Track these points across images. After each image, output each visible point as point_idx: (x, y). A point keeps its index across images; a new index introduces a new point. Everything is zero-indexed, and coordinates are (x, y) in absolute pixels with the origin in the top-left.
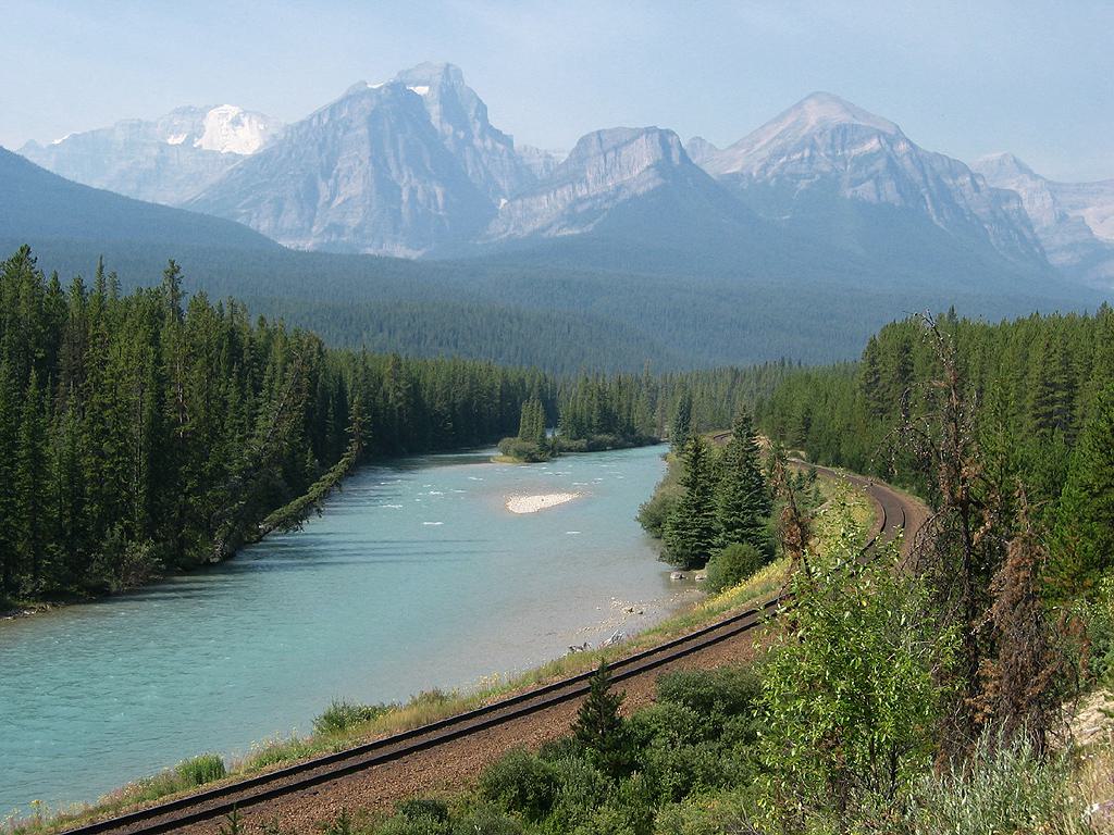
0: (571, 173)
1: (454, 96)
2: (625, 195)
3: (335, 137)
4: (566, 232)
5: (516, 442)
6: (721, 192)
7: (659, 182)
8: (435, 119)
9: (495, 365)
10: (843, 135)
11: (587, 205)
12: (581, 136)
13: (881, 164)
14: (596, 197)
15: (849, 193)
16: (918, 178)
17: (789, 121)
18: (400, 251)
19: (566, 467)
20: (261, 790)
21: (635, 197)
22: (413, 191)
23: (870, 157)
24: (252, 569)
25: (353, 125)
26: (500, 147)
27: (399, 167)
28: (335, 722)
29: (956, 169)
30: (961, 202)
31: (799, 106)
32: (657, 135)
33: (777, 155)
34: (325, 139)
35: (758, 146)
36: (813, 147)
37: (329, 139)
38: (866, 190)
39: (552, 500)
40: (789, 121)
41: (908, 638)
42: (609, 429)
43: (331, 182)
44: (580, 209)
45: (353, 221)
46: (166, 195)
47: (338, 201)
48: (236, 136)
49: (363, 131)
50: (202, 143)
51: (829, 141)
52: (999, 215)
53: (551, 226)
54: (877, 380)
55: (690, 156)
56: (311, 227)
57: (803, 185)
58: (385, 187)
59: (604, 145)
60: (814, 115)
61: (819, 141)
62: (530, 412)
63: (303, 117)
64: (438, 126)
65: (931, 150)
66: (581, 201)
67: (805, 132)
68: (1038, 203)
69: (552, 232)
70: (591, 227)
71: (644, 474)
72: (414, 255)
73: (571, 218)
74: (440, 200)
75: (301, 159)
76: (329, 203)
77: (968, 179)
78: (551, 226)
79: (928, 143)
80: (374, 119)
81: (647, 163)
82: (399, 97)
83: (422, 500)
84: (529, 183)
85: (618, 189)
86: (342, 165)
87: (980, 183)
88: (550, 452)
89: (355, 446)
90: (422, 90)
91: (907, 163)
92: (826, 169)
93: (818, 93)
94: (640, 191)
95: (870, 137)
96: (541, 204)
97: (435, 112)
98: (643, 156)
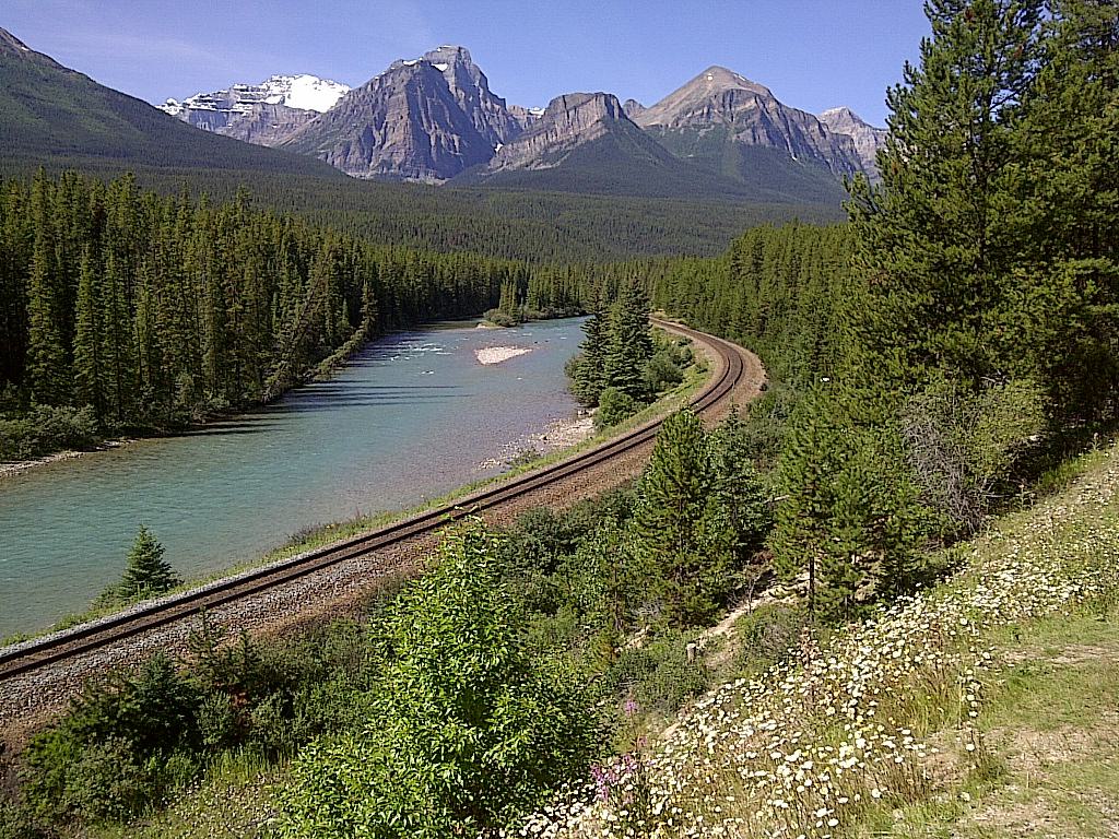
2: (581, 140)
3: (383, 99)
5: (497, 313)
6: (647, 139)
7: (604, 131)
8: (452, 88)
9: (450, 264)
10: (730, 97)
11: (556, 148)
13: (756, 118)
14: (562, 143)
16: (782, 127)
19: (529, 331)
22: (438, 138)
23: (749, 113)
24: (298, 409)
25: (396, 91)
26: (497, 107)
27: (429, 121)
28: (300, 540)
29: (808, 119)
30: (811, 144)
31: (701, 76)
32: (603, 98)
34: (377, 100)
35: (672, 106)
36: (710, 106)
37: (380, 101)
38: (746, 137)
39: (522, 352)
40: (693, 88)
42: (562, 306)
43: (382, 132)
44: (551, 151)
45: (398, 159)
47: (387, 144)
48: (314, 95)
49: (402, 96)
51: (721, 101)
52: (838, 152)
54: (739, 271)
55: (626, 112)
56: (370, 162)
57: (702, 133)
58: (419, 136)
59: (566, 105)
60: (712, 84)
61: (714, 102)
62: (507, 292)
63: (361, 85)
64: (454, 92)
66: (553, 145)
67: (705, 95)
68: (865, 143)
71: (569, 337)
73: (545, 156)
74: (456, 144)
77: (817, 127)
80: (410, 87)
81: (596, 119)
82: (427, 66)
83: (429, 350)
84: (515, 131)
86: (389, 119)
87: (825, 130)
88: (521, 320)
89: (367, 321)
90: (442, 67)
91: (775, 116)
93: (714, 67)
94: (592, 139)
95: (749, 98)
96: (524, 147)
97: (451, 80)
98: (595, 111)
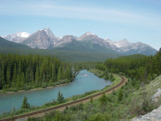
0: (62, 40)
1: (49, 31)
2: (68, 42)
4: (62, 46)
6: (78, 42)
7: (72, 41)
12: (64, 36)
15: (92, 43)
17: (85, 35)
18: (44, 48)
20: (8, 120)
21: (69, 43)
32: (71, 36)
33: (84, 38)
40: (85, 35)
41: (68, 115)
44: (63, 44)
46: (17, 42)
48: (25, 35)
50: (21, 36)
53: (60, 46)
57: (87, 41)
65: (100, 38)
66: (63, 43)
69: (60, 46)
70: (64, 46)
72: (45, 49)
75: (32, 38)
76: (36, 43)
78: (60, 46)
79: (100, 37)
82: (43, 32)
84: (56, 39)
85: (67, 42)
90: (46, 31)
92: (89, 40)
94: (70, 42)
98: (70, 38)
